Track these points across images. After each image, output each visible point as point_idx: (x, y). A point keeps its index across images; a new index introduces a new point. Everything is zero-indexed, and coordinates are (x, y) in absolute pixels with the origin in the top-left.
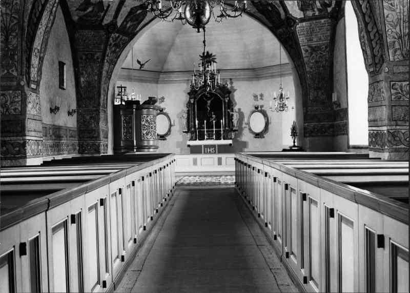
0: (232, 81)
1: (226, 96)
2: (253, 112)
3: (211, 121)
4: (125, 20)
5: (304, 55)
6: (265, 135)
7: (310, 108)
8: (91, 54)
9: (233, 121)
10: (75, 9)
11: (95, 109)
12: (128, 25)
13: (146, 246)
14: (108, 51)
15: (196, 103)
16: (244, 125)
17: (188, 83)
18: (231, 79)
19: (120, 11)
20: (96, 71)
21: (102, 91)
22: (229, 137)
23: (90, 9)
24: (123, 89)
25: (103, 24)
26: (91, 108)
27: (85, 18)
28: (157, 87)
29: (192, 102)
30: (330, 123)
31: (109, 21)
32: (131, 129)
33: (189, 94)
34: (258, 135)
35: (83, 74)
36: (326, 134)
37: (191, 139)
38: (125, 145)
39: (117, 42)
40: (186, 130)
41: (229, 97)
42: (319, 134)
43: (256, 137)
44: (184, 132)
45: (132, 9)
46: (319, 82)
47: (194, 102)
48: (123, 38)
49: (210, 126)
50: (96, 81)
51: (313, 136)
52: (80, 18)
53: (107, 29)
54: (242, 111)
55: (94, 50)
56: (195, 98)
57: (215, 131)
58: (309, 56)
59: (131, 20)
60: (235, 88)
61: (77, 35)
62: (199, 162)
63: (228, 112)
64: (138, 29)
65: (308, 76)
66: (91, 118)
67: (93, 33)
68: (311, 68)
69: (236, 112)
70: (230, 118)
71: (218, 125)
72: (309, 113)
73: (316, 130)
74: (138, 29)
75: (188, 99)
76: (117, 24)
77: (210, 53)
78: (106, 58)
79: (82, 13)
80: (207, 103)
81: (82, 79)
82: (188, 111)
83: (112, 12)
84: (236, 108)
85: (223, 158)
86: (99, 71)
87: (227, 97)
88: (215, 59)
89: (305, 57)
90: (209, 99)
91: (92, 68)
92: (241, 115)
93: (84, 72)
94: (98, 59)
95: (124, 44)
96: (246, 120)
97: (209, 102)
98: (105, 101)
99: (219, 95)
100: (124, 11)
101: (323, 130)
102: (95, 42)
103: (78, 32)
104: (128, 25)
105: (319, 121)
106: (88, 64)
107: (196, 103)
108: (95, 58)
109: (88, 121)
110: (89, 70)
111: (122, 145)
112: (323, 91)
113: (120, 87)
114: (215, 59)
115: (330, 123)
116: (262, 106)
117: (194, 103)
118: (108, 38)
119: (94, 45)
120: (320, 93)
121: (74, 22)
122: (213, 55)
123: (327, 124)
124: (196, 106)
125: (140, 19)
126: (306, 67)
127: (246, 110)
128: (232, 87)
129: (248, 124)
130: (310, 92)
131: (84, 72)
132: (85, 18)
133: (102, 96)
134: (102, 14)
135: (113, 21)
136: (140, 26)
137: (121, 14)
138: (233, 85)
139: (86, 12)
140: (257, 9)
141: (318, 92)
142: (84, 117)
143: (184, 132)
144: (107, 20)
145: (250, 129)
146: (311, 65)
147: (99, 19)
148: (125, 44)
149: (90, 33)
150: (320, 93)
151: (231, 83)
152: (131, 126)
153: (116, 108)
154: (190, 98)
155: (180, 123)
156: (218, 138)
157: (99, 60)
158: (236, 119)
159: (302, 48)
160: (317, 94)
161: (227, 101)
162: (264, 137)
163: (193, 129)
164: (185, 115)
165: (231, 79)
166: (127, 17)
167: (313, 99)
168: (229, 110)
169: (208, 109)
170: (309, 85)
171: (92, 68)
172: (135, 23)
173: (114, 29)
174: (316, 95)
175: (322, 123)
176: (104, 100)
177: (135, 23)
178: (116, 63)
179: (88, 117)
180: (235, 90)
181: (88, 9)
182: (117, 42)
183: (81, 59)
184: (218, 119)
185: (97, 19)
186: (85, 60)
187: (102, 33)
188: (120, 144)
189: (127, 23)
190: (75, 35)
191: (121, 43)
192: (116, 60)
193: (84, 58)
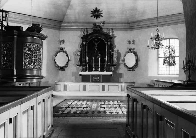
1: (109, 40)
2: (127, 53)
6: (135, 69)
16: (121, 62)
18: (112, 29)
32: (12, 58)
33: (82, 38)
43: (129, 70)
44: (78, 65)
47: (86, 44)
49: (96, 61)
60: (115, 35)
70: (111, 56)
71: (102, 61)
75: (82, 42)
82: (81, 50)
84: (115, 49)
87: (109, 41)
90: (97, 42)
96: (122, 58)
97: (96, 44)
116: (134, 49)
117: (85, 45)
128: (113, 35)
129: (124, 61)
143: (78, 65)
145: (125, 65)
151: (113, 32)
154: (83, 41)
155: (75, 59)
161: (109, 44)
165: (112, 29)
168: (111, 51)
180: (115, 37)
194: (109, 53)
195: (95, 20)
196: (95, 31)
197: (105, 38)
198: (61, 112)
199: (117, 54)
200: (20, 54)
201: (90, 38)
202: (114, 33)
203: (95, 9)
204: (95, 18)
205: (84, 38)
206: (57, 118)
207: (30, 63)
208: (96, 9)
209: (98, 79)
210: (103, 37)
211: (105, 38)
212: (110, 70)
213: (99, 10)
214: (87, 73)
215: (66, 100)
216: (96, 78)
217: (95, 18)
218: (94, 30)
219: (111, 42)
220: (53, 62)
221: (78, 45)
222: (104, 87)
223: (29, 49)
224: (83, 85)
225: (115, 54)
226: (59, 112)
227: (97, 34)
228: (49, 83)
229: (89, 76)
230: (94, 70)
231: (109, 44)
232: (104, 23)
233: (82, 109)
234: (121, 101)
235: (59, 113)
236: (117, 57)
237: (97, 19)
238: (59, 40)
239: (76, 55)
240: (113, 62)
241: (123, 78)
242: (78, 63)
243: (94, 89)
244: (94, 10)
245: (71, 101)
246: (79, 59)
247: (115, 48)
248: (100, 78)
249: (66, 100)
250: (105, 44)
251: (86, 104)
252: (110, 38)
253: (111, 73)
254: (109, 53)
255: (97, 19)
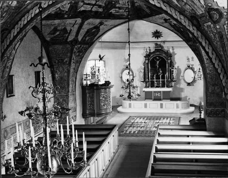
0: (174, 48)
1: (169, 59)
2: (186, 70)
3: (159, 74)
4: (85, 36)
5: (206, 62)
6: (194, 84)
7: (209, 98)
8: (62, 59)
9: (173, 75)
10: (47, 34)
11: (66, 94)
12: (87, 39)
13: (113, 161)
14: (74, 56)
15: (149, 63)
16: (181, 78)
17: (144, 50)
18: (173, 47)
19: (79, 32)
20: (65, 70)
21: (70, 82)
22: (170, 85)
23: (58, 33)
24: (88, 75)
25: (68, 41)
26: (63, 94)
27: (55, 38)
28: (125, 52)
29: (147, 62)
30: (222, 108)
31: (72, 39)
32: (94, 103)
33: (145, 57)
34: (189, 84)
35: (57, 72)
36: (220, 115)
37: (146, 87)
38: (89, 113)
39: (80, 49)
40: (143, 81)
41: (171, 59)
42: (215, 116)
43: (188, 86)
44: (141, 81)
45: (88, 30)
46: (216, 80)
47: (148, 62)
48: (84, 47)
49: (158, 78)
50: (66, 76)
51: (210, 117)
52: (52, 39)
53: (72, 43)
54: (180, 67)
55: (63, 57)
56: (148, 60)
57: (162, 81)
58: (209, 63)
59: (88, 36)
60: (175, 53)
61: (51, 49)
62: (148, 105)
63: (170, 69)
64: (95, 40)
65: (208, 76)
66: (63, 100)
67: (61, 47)
68: (211, 71)
69: (175, 69)
70: (171, 73)
71: (163, 77)
72: (208, 101)
73: (213, 113)
74: (95, 40)
75: (144, 60)
76: (78, 40)
77: (158, 31)
78: (72, 61)
79: (52, 36)
80: (157, 63)
81: (57, 75)
82: (145, 68)
83: (74, 34)
84: (176, 66)
85: (163, 104)
86: (68, 70)
87: (169, 59)
88: (162, 34)
89: (206, 63)
90: (158, 60)
91: (63, 68)
92: (179, 70)
93: (58, 71)
94: (66, 62)
95: (86, 49)
96: (182, 74)
97: (158, 62)
98: (74, 87)
99: (164, 58)
100: (82, 32)
101: (218, 113)
102: (64, 52)
103: (51, 47)
104: (87, 39)
105: (215, 106)
106: (60, 65)
107: (149, 63)
108: (65, 62)
109: (61, 102)
110: (61, 69)
111: (87, 113)
112: (218, 87)
113: (85, 75)
114: (162, 34)
115: (222, 108)
116: (192, 65)
117: (148, 63)
118: (72, 50)
119: (63, 53)
120: (216, 88)
121: (48, 41)
122: (160, 32)
123: (220, 109)
124: (149, 65)
125: (95, 34)
126: (207, 70)
127: (183, 68)
128: (174, 52)
129: (183, 76)
130: (209, 87)
131: (58, 71)
132: (55, 38)
133: (71, 86)
134: (67, 35)
135: (75, 38)
136: (96, 38)
137: (81, 34)
138: (174, 51)
139: (55, 35)
140: (174, 28)
141: (215, 87)
142: (58, 100)
143: (141, 81)
144: (71, 38)
145: (184, 80)
146: (210, 69)
147: (65, 38)
148: (86, 50)
149: (59, 47)
150: (216, 88)
151: (173, 49)
152: (93, 100)
153: (84, 88)
154: (146, 60)
155: (139, 76)
156: (163, 86)
157: (68, 63)
158: (175, 74)
159: (204, 57)
160: (214, 89)
161: (169, 62)
162: (194, 85)
163: (147, 80)
164: (143, 71)
165: (173, 47)
166: (85, 35)
167: (211, 92)
168: (170, 68)
169: (157, 67)
170: (209, 82)
171: (63, 68)
172: (92, 37)
173: (77, 42)
174: (213, 89)
175: (217, 108)
176: (72, 87)
177: (92, 37)
178: (80, 62)
179: (61, 100)
180: (176, 54)
181: (56, 33)
182: (80, 49)
183: (55, 63)
184: (164, 73)
185: (63, 38)
186: (58, 63)
187: (68, 46)
188: (86, 112)
189: (86, 38)
190: (49, 49)
191: (83, 50)
192: (80, 60)
193: (56, 62)
194: (169, 70)
195: (156, 40)
196: (157, 50)
197: (166, 56)
198: (125, 132)
199: (177, 71)
200: (99, 101)
201: (152, 57)
202: (175, 51)
203: (155, 31)
204: (156, 38)
205: (147, 56)
206: (121, 138)
207: (104, 105)
208: (157, 31)
209: (159, 95)
210: (164, 55)
211: (166, 56)
212: (170, 85)
213: (159, 32)
214: (150, 89)
215: (131, 117)
216: (157, 94)
217: (156, 38)
218: (155, 49)
219: (171, 60)
220: (120, 79)
221: (142, 62)
222: (162, 105)
223: (104, 97)
224: (145, 104)
225: (174, 70)
226: (123, 132)
227: (158, 53)
228: (117, 97)
229: (151, 92)
230: (156, 86)
231: (169, 62)
232: (164, 42)
233: (140, 128)
234: (174, 118)
235: (124, 133)
236: (177, 74)
237: (158, 39)
238: (125, 58)
239: (140, 72)
240: (173, 78)
241: (184, 92)
242: (142, 80)
243: (153, 107)
244: (155, 32)
245: (134, 119)
246: (142, 76)
247: (175, 65)
248: (161, 94)
249: (130, 116)
250: (166, 61)
251: (145, 123)
252: (170, 56)
253: (170, 89)
254: (169, 70)
255: (158, 39)
